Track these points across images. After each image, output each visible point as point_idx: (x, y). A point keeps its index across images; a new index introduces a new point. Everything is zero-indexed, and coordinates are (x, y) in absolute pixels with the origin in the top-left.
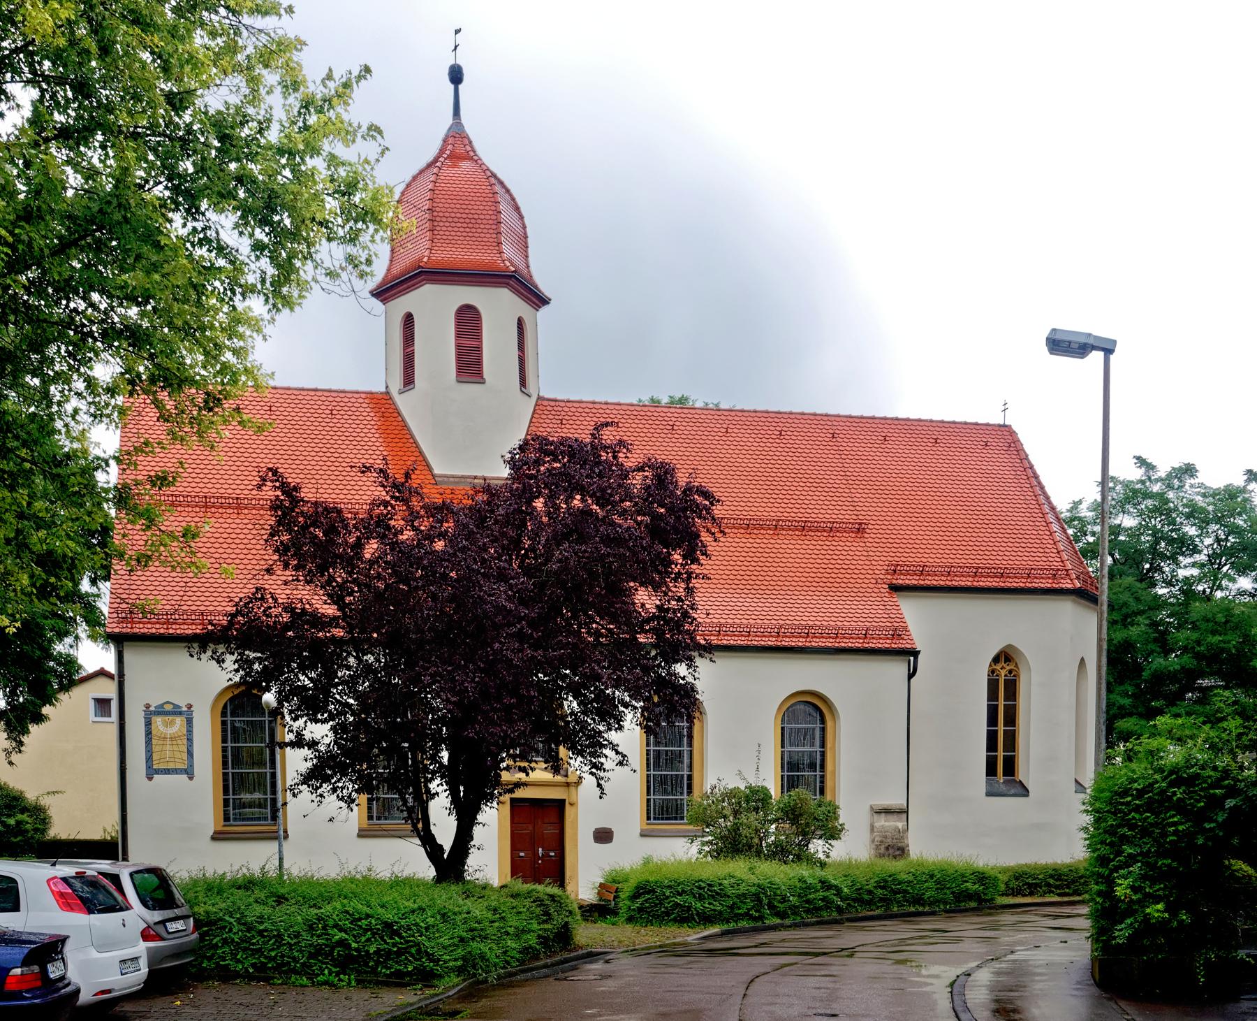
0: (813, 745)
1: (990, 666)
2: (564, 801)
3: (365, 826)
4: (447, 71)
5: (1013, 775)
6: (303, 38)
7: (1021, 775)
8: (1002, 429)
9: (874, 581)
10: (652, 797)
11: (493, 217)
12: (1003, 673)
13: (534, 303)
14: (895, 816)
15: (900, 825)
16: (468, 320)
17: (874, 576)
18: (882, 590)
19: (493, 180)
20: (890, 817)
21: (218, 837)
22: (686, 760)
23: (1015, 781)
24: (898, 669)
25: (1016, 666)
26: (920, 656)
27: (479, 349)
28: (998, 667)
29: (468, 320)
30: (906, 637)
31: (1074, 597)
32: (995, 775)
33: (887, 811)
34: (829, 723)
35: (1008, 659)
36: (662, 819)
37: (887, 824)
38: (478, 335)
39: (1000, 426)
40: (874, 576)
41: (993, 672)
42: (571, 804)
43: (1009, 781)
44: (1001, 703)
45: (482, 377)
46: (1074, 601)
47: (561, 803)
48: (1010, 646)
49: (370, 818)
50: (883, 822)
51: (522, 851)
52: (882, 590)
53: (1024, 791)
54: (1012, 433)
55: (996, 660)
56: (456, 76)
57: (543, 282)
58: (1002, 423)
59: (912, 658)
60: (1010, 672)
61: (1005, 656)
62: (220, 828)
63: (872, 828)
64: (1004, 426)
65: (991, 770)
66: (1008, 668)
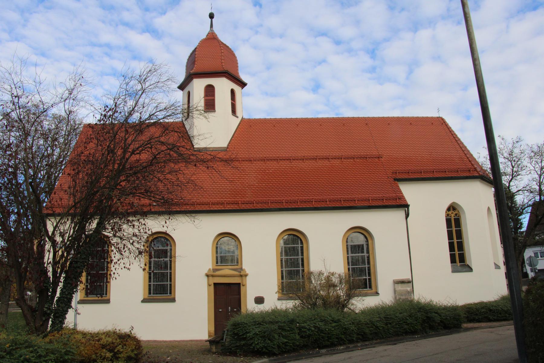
0: (363, 252)
1: (446, 212)
2: (240, 284)
3: (146, 297)
4: (209, 15)
5: (464, 262)
6: (487, 208)
7: (468, 262)
8: (439, 118)
9: (387, 177)
10: (367, 277)
11: (220, 54)
12: (453, 215)
13: (239, 84)
14: (406, 285)
15: (409, 289)
16: (210, 91)
17: (387, 176)
18: (391, 181)
19: (220, 43)
20: (403, 285)
21: (144, 301)
22: (169, 254)
23: (465, 265)
24: (401, 213)
25: (458, 212)
26: (410, 208)
27: (214, 100)
28: (450, 213)
29: (210, 91)
30: (403, 200)
31: (480, 179)
32: (455, 262)
33: (402, 282)
34: (370, 242)
35: (454, 209)
36: (163, 294)
37: (402, 289)
38: (213, 95)
39: (437, 117)
40: (387, 176)
41: (448, 215)
42: (243, 285)
43: (462, 265)
44: (454, 229)
45: (215, 110)
46: (480, 181)
47: (239, 284)
48: (454, 203)
49: (150, 293)
50: (400, 287)
51: (221, 309)
52: (391, 181)
53: (470, 269)
54: (443, 119)
55: (449, 209)
56: (211, 16)
57: (244, 77)
58: (438, 116)
59: (406, 209)
60: (456, 215)
61: (452, 207)
62: (82, 298)
63: (395, 291)
64: (439, 117)
65: (453, 261)
66: (455, 213)
